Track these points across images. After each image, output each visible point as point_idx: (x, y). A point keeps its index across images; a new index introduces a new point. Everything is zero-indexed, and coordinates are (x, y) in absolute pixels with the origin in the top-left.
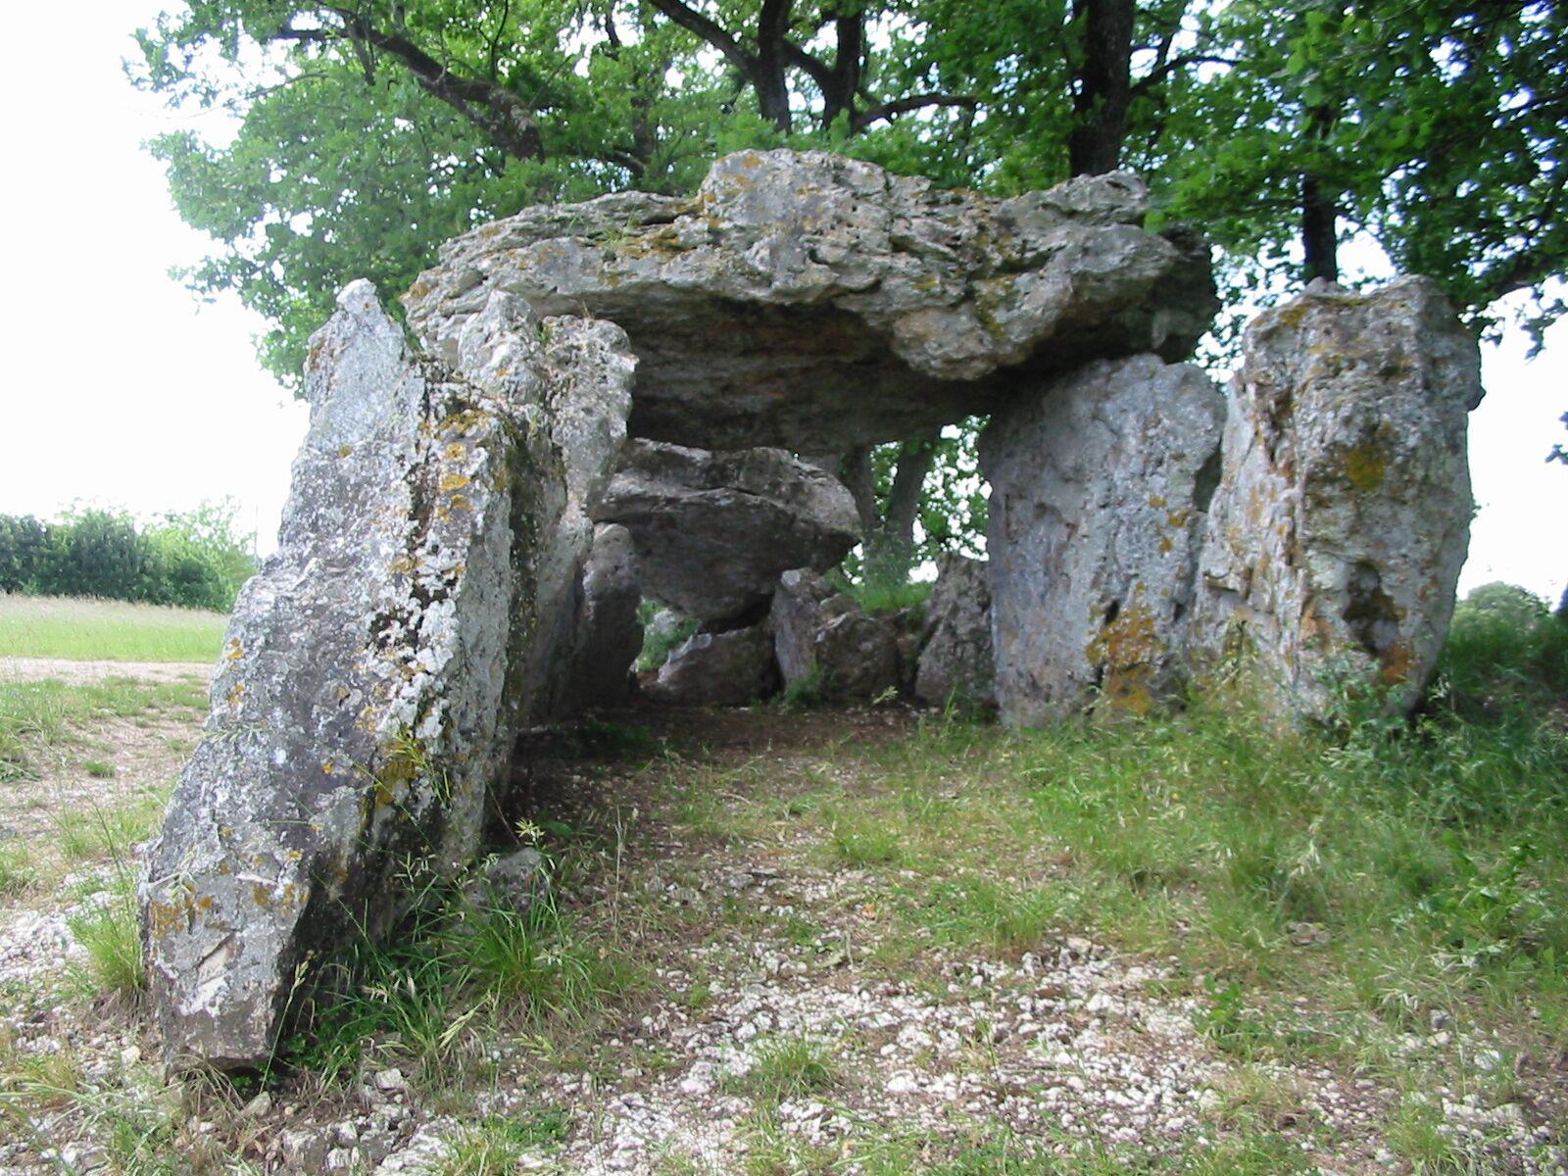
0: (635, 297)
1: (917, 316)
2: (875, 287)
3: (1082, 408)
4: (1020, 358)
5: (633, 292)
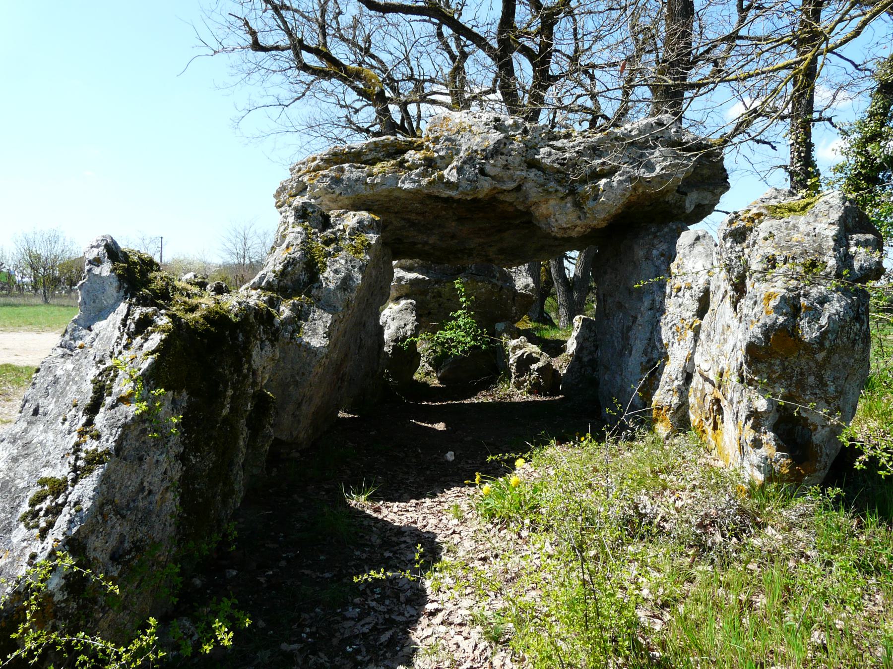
0: (386, 196)
1: (849, 35)
2: (518, 188)
3: (640, 253)
4: (604, 224)
5: (384, 194)
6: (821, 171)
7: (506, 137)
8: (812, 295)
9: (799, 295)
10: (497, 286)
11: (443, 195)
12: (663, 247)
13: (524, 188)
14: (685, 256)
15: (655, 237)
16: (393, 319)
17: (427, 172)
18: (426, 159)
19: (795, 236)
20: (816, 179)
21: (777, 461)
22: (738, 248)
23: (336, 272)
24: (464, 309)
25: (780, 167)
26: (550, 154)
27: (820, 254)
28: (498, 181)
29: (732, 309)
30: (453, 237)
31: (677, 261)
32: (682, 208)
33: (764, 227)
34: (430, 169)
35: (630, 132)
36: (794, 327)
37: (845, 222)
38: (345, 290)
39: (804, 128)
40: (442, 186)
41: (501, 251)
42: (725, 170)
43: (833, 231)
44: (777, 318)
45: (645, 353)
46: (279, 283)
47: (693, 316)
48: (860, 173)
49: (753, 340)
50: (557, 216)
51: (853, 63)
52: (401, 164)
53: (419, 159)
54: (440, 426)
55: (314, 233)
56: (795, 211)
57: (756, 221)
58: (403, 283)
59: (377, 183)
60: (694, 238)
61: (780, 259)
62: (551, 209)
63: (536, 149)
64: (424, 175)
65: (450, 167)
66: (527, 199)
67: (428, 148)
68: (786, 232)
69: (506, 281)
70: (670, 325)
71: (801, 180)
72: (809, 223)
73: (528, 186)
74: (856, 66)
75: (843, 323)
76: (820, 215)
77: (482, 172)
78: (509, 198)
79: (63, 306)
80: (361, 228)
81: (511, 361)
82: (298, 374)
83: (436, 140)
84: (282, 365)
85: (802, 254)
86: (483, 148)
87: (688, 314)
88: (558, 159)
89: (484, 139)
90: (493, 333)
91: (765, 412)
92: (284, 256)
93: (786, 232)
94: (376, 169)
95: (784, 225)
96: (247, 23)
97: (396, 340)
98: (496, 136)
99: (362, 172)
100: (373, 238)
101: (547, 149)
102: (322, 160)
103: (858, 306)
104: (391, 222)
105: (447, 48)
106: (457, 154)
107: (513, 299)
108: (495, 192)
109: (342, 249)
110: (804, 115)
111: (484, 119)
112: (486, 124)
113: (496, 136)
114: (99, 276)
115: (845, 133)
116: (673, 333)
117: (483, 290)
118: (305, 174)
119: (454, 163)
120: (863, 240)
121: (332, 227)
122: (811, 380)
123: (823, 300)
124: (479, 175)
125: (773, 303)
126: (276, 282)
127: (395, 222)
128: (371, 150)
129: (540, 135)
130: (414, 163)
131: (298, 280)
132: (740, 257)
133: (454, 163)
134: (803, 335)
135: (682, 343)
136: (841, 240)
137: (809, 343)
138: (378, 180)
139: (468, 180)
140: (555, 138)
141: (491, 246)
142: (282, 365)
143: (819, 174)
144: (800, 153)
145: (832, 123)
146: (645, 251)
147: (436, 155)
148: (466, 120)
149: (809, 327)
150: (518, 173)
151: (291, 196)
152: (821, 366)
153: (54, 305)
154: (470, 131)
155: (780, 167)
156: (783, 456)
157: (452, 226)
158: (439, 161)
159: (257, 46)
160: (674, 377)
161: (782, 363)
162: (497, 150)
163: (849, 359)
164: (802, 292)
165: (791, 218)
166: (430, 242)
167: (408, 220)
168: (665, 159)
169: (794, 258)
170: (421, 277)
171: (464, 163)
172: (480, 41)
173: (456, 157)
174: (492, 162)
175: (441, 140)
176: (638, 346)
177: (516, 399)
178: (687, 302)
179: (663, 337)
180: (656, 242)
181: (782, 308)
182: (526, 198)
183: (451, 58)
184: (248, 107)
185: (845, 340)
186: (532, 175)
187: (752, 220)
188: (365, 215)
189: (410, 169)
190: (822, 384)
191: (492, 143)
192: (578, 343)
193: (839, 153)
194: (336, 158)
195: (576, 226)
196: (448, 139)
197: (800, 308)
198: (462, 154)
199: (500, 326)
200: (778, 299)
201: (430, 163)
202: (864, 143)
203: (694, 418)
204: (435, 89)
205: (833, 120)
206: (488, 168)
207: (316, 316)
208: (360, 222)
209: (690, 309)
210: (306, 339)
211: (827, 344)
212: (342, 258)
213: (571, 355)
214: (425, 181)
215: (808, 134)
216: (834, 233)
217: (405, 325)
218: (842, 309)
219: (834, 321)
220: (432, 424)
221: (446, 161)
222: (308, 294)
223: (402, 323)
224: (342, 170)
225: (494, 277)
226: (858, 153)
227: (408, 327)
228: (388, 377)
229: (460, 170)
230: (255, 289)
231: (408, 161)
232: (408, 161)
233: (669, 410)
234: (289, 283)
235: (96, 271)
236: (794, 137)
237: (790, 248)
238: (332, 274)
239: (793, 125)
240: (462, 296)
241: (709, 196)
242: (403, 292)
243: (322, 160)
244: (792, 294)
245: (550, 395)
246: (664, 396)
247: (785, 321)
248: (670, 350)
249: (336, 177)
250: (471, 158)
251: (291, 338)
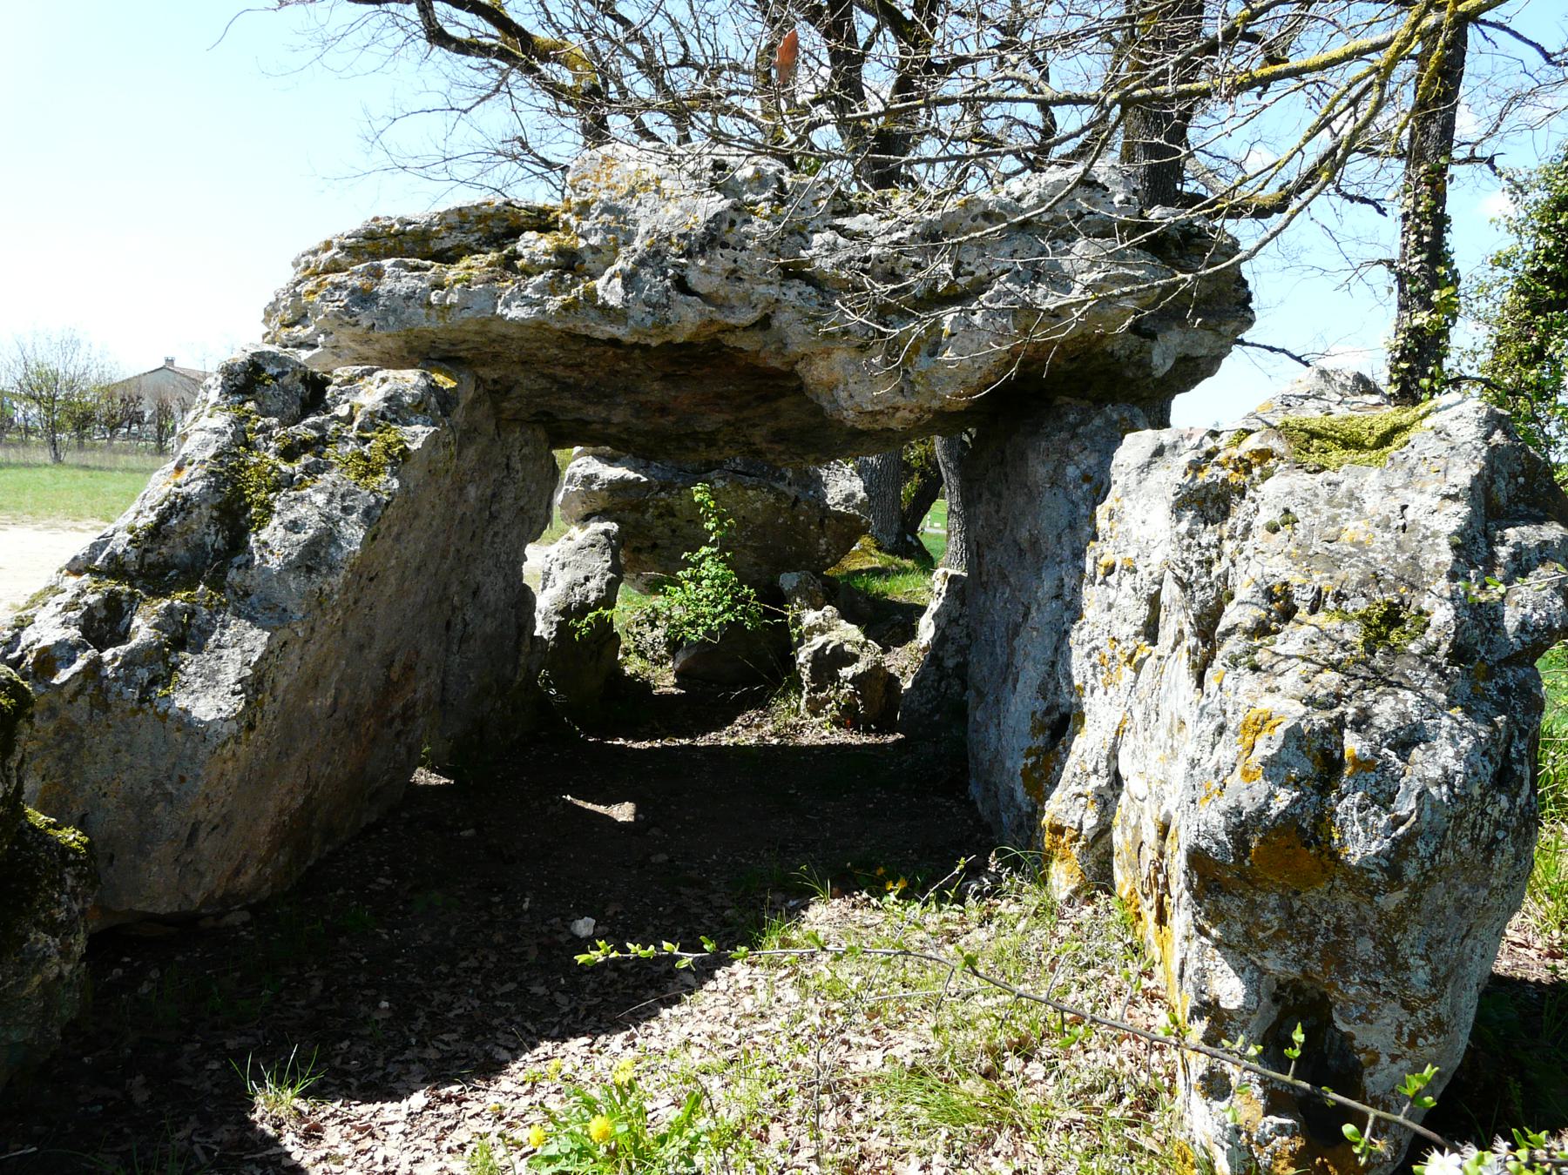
0: (476, 333)
2: (764, 323)
3: (1040, 470)
5: (472, 327)
6: (1462, 274)
7: (735, 208)
8: (1377, 722)
9: (1340, 723)
10: (788, 497)
11: (597, 335)
12: (1089, 460)
13: (775, 323)
14: (1126, 493)
15: (1074, 436)
16: (564, 566)
17: (562, 281)
18: (560, 252)
19: (1350, 525)
20: (1451, 290)
21: (1264, 1142)
22: (1208, 536)
24: (714, 544)
25: (1380, 262)
26: (833, 248)
27: (1413, 587)
28: (719, 307)
29: (1191, 682)
30: (663, 410)
31: (1109, 502)
32: (1145, 365)
33: (1276, 491)
34: (568, 276)
35: (1019, 200)
36: (1320, 818)
37: (1487, 491)
38: (310, 570)
39: (1432, 183)
40: (593, 313)
41: (779, 436)
42: (1245, 283)
43: (1451, 519)
44: (1271, 795)
45: (1042, 691)
46: (141, 557)
47: (1137, 634)
48: (1543, 270)
49: (1203, 844)
50: (851, 386)
51: (1541, 50)
52: (509, 262)
53: (546, 253)
54: (623, 812)
55: (265, 429)
56: (1360, 446)
57: (1256, 471)
58: (595, 487)
59: (452, 305)
60: (1152, 449)
61: (1303, 598)
62: (838, 368)
63: (801, 233)
64: (553, 288)
65: (610, 271)
66: (785, 345)
68: (1327, 511)
69: (806, 487)
70: (1087, 648)
71: (1419, 291)
72: (1390, 490)
73: (783, 318)
74: (1547, 57)
75: (1460, 807)
76: (1421, 469)
77: (681, 285)
78: (748, 343)
79: (86, 467)
80: (396, 410)
81: (801, 659)
82: (169, 778)
83: (584, 210)
84: (127, 759)
85: (1362, 583)
86: (684, 230)
87: (1125, 630)
88: (850, 259)
90: (775, 597)
91: (1239, 1011)
92: (165, 490)
93: (1327, 511)
94: (453, 272)
95: (1324, 492)
97: (566, 612)
98: (717, 203)
99: (421, 278)
100: (417, 435)
101: (829, 236)
102: (342, 247)
103: (1510, 740)
104: (517, 382)
107: (822, 521)
108: (714, 329)
109: (330, 466)
110: (1431, 147)
113: (717, 203)
115: (1518, 189)
116: (1094, 666)
117: (758, 505)
119: (619, 264)
120: (1532, 543)
121: (327, 410)
122: (1365, 947)
123: (1408, 739)
124: (673, 293)
125: (1265, 748)
126: (132, 556)
127: (525, 382)
128: (450, 228)
129: (815, 202)
130: (533, 262)
131: (201, 546)
132: (1210, 562)
134: (1342, 845)
135: (1111, 691)
136: (1473, 549)
137: (1359, 868)
138: (453, 298)
139: (647, 303)
140: (849, 211)
141: (754, 426)
142: (127, 759)
143: (1458, 281)
144: (1420, 234)
145: (1494, 168)
146: (1050, 466)
147: (582, 243)
149: (1364, 821)
150: (761, 289)
152: (1397, 922)
153: (71, 466)
154: (658, 191)
155: (1380, 262)
156: (1281, 1130)
157: (655, 390)
158: (588, 256)
160: (1090, 768)
161: (1285, 905)
162: (713, 238)
163: (1475, 887)
164: (1351, 711)
165: (1351, 473)
166: (615, 420)
167: (553, 379)
169: (1340, 597)
170: (632, 475)
171: (641, 263)
173: (623, 250)
174: (702, 262)
175: (595, 210)
176: (1031, 674)
177: (808, 738)
178: (1126, 602)
179: (1074, 672)
180: (1073, 447)
181: (1287, 764)
182: (783, 344)
185: (1465, 846)
186: (792, 295)
187: (1244, 466)
188: (410, 379)
190: (1393, 961)
191: (702, 219)
192: (937, 627)
193: (1503, 229)
194: (377, 243)
195: (897, 409)
196: (607, 209)
197: (1340, 764)
198: (637, 243)
199: (788, 581)
200: (1279, 732)
201: (569, 263)
202: (1554, 211)
203: (1122, 877)
205: (1498, 162)
206: (693, 278)
207: (227, 637)
209: (1130, 618)
210: (181, 701)
211: (1411, 871)
212: (321, 490)
213: (924, 650)
214: (554, 303)
215: (1439, 197)
216: (1454, 524)
217: (587, 579)
218: (1460, 767)
219: (1436, 805)
220: (608, 804)
222: (217, 584)
223: (581, 575)
224: (377, 274)
225: (783, 477)
226: (1541, 230)
227: (592, 584)
228: (548, 686)
229: (629, 280)
230: (78, 573)
232: (521, 257)
233: (1076, 839)
234: (181, 552)
236: (1410, 202)
237: (1333, 562)
238: (281, 532)
239: (1410, 178)
240: (708, 520)
241: (1209, 338)
242: (598, 505)
243: (342, 247)
244: (1320, 718)
245: (878, 732)
246: (1065, 806)
247: (1294, 802)
248: (1088, 701)
249: (362, 290)
250: (657, 253)
251: (142, 700)
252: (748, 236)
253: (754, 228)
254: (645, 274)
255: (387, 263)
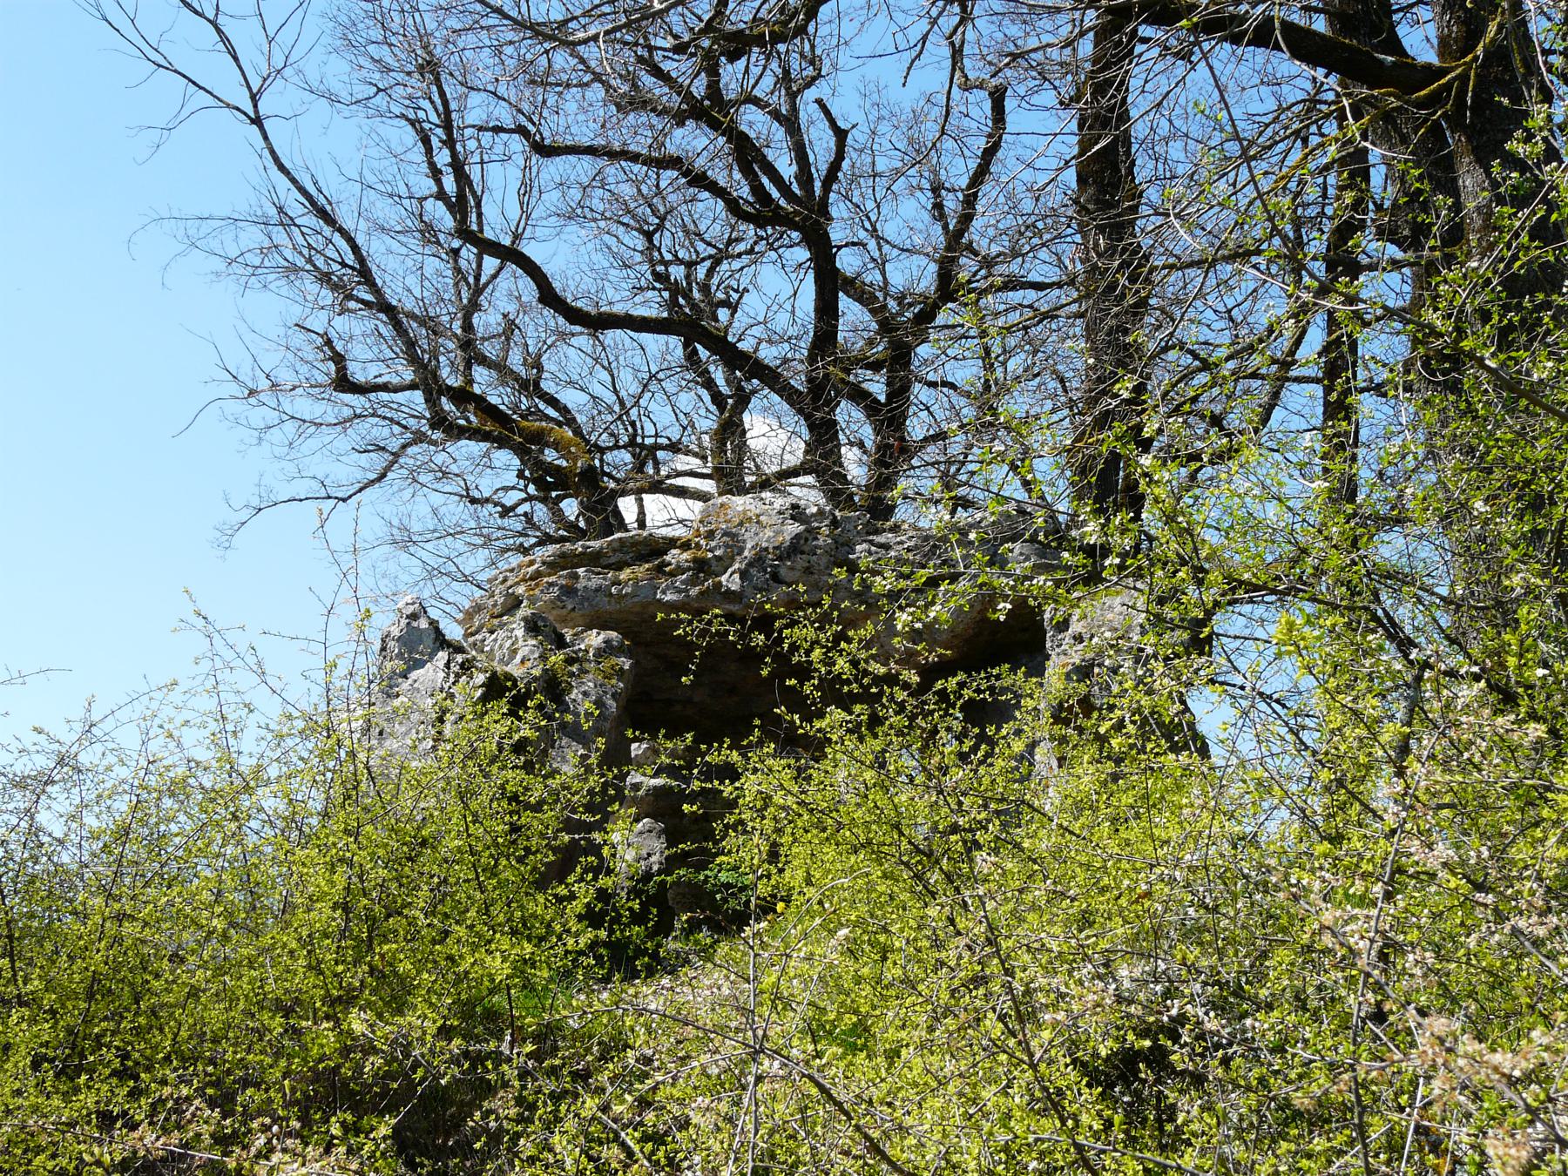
0: (637, 613)
23: (585, 694)
52: (660, 569)
64: (693, 582)
67: (698, 546)
80: (607, 650)
83: (710, 535)
89: (777, 533)
94: (624, 575)
96: (329, 342)
101: (865, 546)
102: (544, 563)
105: (709, 384)
106: (740, 554)
109: (587, 672)
111: (777, 506)
112: (780, 513)
113: (793, 528)
114: (418, 629)
118: (517, 584)
119: (737, 566)
128: (614, 551)
133: (737, 566)
147: (710, 555)
148: (752, 507)
151: (493, 617)
158: (714, 563)
159: (343, 383)
162: (796, 547)
168: (1027, 559)
171: (750, 565)
172: (771, 377)
175: (718, 535)
183: (714, 401)
184: (256, 502)
189: (672, 574)
191: (788, 538)
196: (725, 534)
198: (746, 553)
204: (680, 467)
206: (783, 572)
208: (607, 642)
214: (694, 591)
221: (724, 563)
223: (644, 853)
224: (576, 577)
227: (654, 859)
229: (744, 574)
231: (670, 564)
235: (415, 624)
243: (544, 563)
252: (816, 547)
253: (821, 542)
254: (753, 571)
255: (581, 571)
